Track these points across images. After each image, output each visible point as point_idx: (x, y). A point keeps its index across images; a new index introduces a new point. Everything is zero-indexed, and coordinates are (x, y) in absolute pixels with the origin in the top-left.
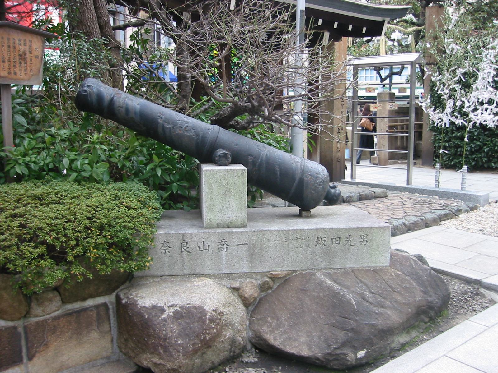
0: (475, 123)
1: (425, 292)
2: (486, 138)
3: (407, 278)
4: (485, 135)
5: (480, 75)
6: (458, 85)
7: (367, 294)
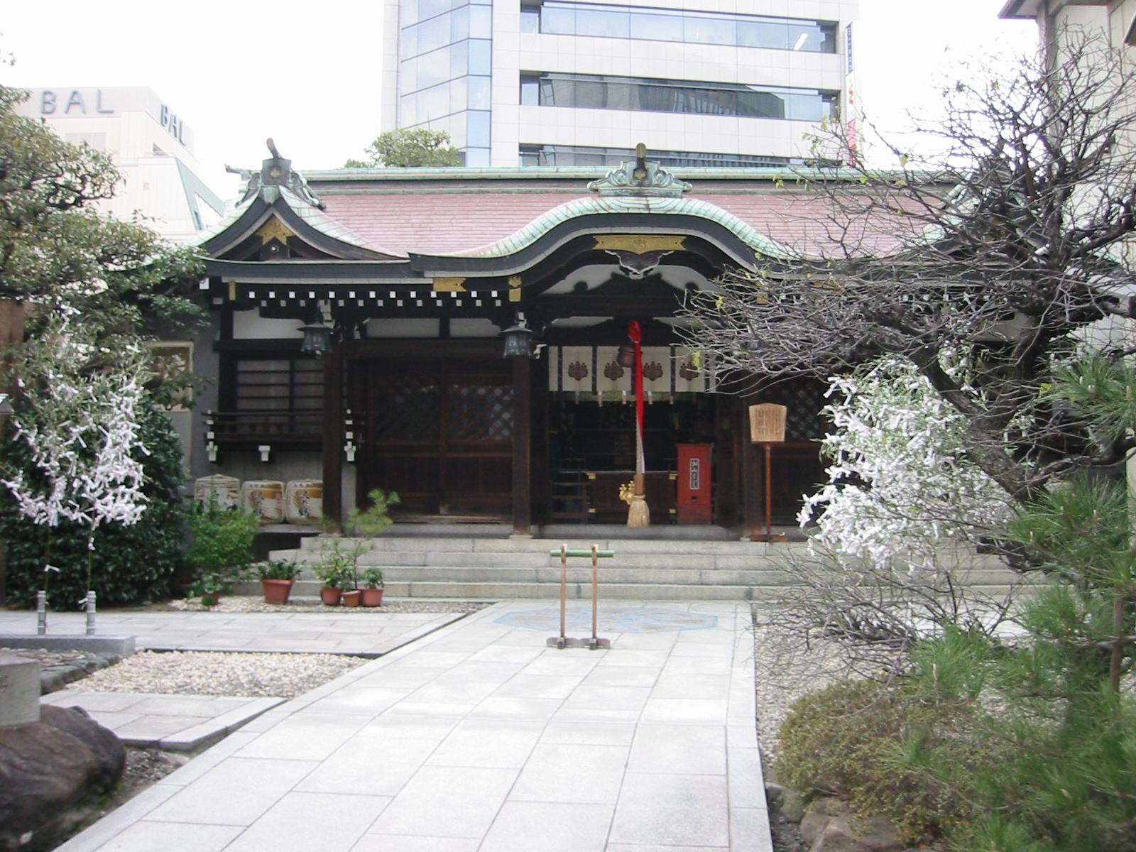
0: (105, 518)
1: (95, 751)
2: (109, 546)
3: (68, 735)
4: (108, 541)
5: (110, 438)
6: (72, 453)
7: (18, 761)
